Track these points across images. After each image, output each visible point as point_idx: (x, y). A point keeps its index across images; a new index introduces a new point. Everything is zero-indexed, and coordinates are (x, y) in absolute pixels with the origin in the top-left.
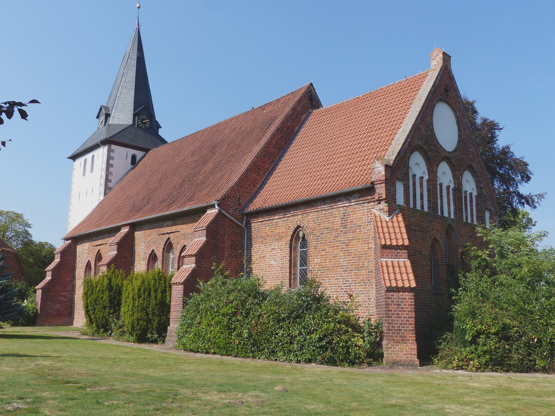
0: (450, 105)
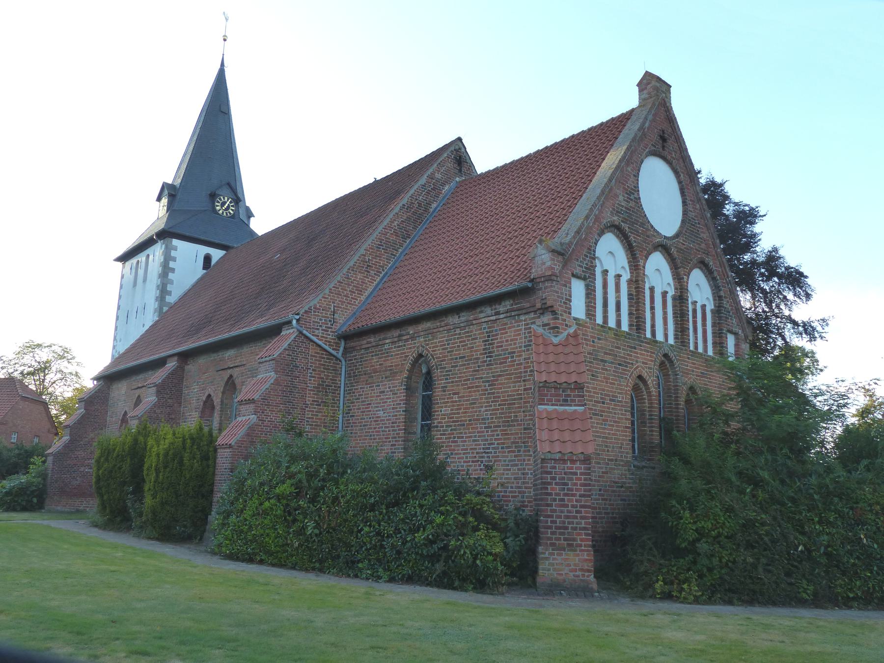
0: (669, 163)
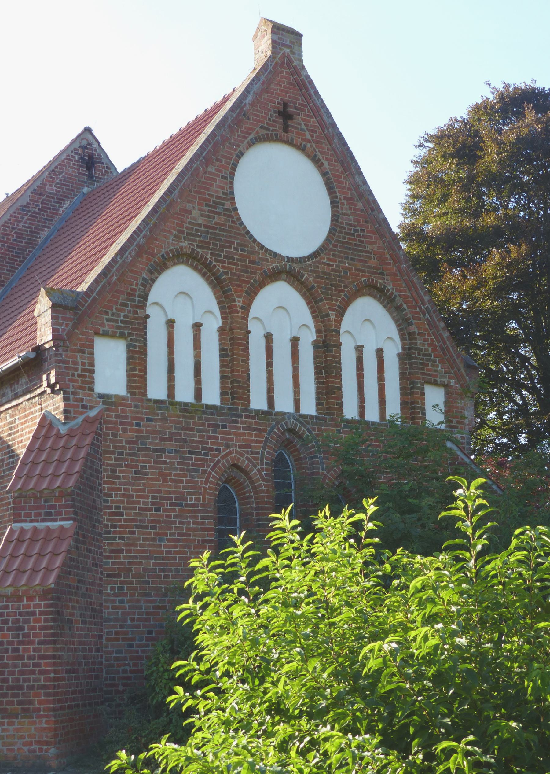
0: (301, 148)
